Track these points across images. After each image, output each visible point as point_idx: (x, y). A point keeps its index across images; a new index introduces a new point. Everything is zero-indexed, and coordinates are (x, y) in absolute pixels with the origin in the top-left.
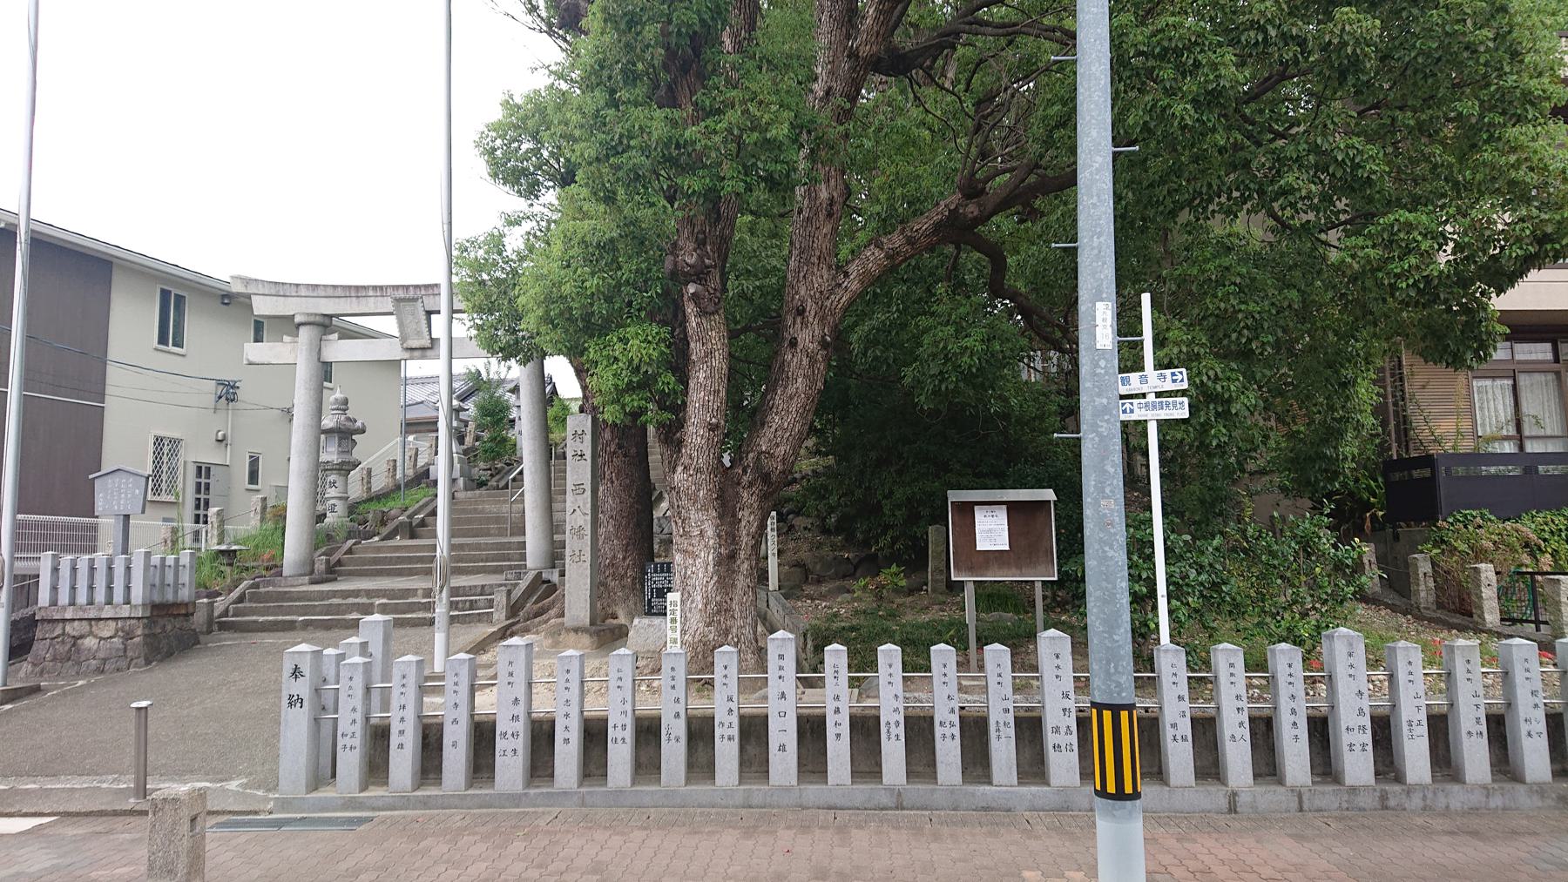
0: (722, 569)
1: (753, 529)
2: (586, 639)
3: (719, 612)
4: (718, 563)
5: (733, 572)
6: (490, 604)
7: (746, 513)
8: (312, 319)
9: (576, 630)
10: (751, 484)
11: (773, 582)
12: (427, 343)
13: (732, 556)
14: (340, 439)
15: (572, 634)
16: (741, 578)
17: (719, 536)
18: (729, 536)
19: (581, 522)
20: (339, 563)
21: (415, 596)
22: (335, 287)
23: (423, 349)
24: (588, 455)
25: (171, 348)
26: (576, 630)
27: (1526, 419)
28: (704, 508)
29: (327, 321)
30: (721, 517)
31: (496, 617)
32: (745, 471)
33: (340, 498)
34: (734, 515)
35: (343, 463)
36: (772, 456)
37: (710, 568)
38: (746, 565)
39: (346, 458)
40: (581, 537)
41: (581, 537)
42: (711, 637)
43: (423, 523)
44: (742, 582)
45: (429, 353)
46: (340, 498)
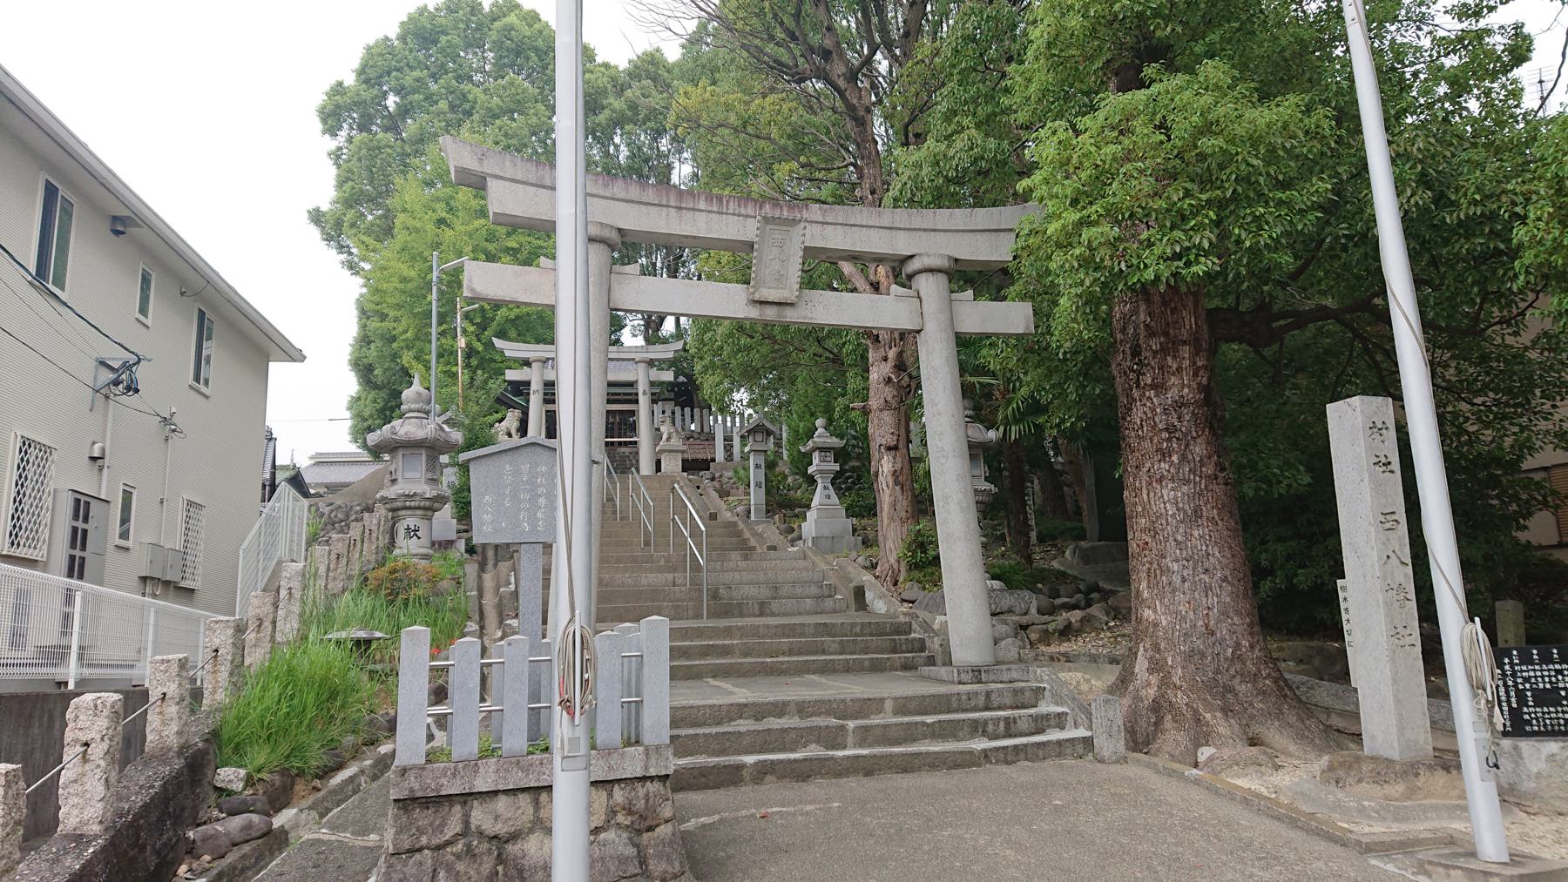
8: (607, 234)
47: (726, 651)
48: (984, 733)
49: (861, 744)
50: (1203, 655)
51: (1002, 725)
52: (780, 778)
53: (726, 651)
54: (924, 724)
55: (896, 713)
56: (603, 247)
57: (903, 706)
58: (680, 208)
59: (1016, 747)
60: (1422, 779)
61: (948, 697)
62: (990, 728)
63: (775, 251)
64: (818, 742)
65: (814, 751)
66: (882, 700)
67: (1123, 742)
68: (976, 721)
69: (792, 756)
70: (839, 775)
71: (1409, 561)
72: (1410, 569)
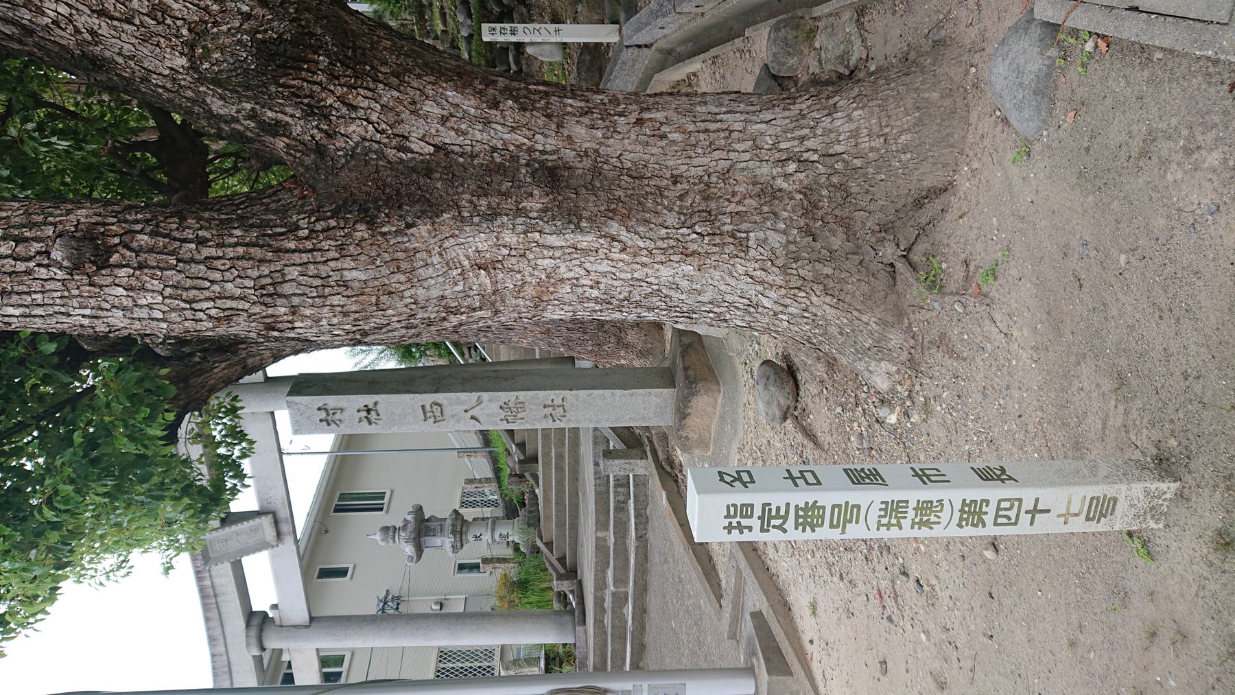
0: (590, 205)
1: (470, 105)
2: (701, 402)
3: (710, 217)
4: (572, 218)
5: (598, 177)
6: (622, 483)
7: (415, 129)
8: (254, 641)
9: (682, 414)
10: (315, 110)
11: (604, 34)
12: (266, 521)
13: (552, 176)
14: (426, 535)
15: (688, 421)
16: (615, 146)
17: (492, 215)
18: (491, 184)
19: (495, 407)
20: (562, 560)
21: (604, 539)
22: (207, 620)
23: (276, 522)
24: (369, 400)
25: (344, 669)
26: (682, 414)
27: (677, 682)
28: (406, 264)
29: (256, 621)
30: (431, 209)
31: (641, 471)
32: (277, 128)
33: (493, 530)
34: (426, 169)
35: (454, 532)
36: (199, 32)
37: (586, 240)
38: (579, 131)
39: (448, 525)
40: (521, 406)
41: (521, 406)
42: (776, 239)
43: (522, 446)
44: (626, 146)
45: (283, 513)
46: (493, 530)
47: (560, 457)
48: (625, 502)
49: (626, 583)
50: (569, 340)
51: (620, 490)
52: (641, 659)
53: (560, 457)
54: (615, 544)
55: (606, 528)
56: (264, 634)
57: (602, 524)
58: (215, 595)
59: (636, 517)
60: (691, 435)
61: (597, 493)
62: (621, 498)
63: (230, 543)
64: (621, 608)
65: (629, 609)
66: (597, 538)
67: (638, 461)
68: (616, 509)
69: (632, 562)
70: (644, 629)
71: (474, 396)
72: (485, 396)
